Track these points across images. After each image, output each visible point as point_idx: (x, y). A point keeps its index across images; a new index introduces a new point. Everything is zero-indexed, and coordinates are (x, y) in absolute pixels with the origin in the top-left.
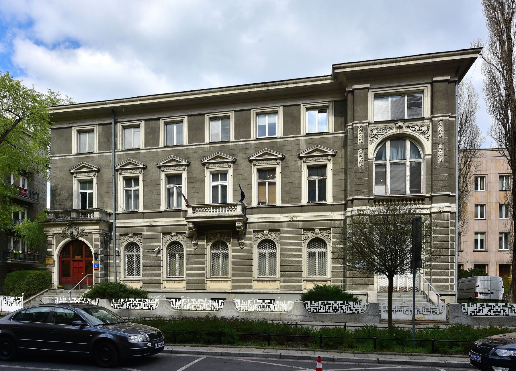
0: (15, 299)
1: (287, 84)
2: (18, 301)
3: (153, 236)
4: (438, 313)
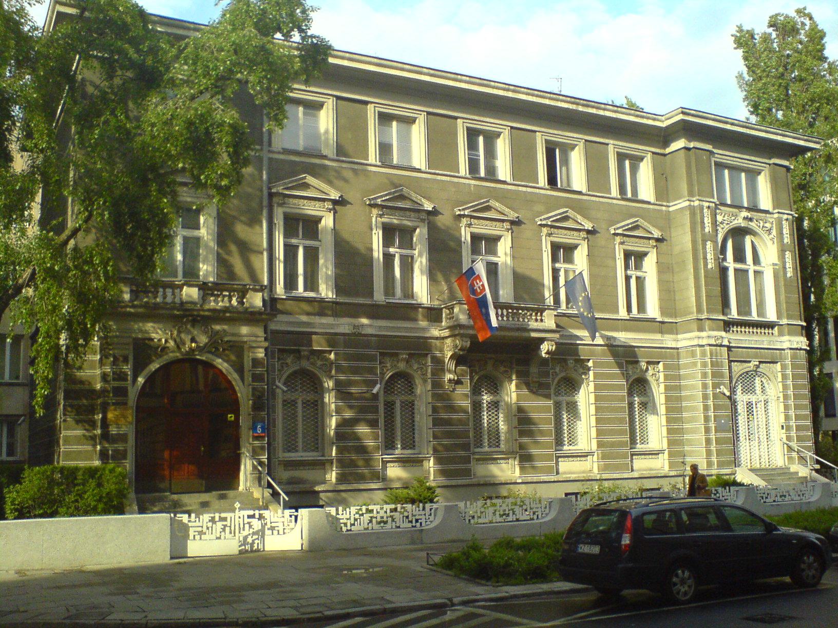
0: (212, 520)
2: (219, 525)
4: (281, 532)
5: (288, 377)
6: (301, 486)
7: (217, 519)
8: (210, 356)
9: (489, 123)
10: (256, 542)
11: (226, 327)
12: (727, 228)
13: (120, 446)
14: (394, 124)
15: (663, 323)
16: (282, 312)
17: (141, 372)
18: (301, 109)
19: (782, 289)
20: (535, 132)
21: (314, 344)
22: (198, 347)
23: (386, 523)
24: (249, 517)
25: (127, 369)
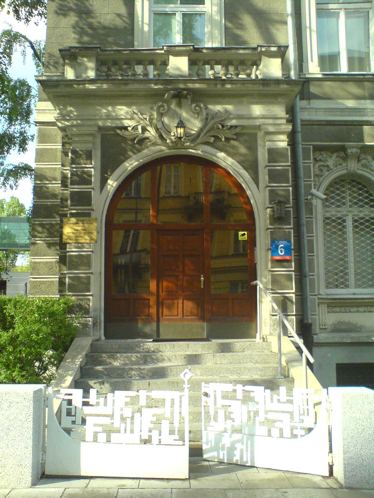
5: (330, 185)
6: (353, 335)
8: (208, 149)
10: (238, 446)
11: (230, 107)
13: (81, 273)
16: (317, 97)
17: (112, 172)
21: (366, 138)
22: (186, 134)
24: (225, 397)
25: (92, 168)
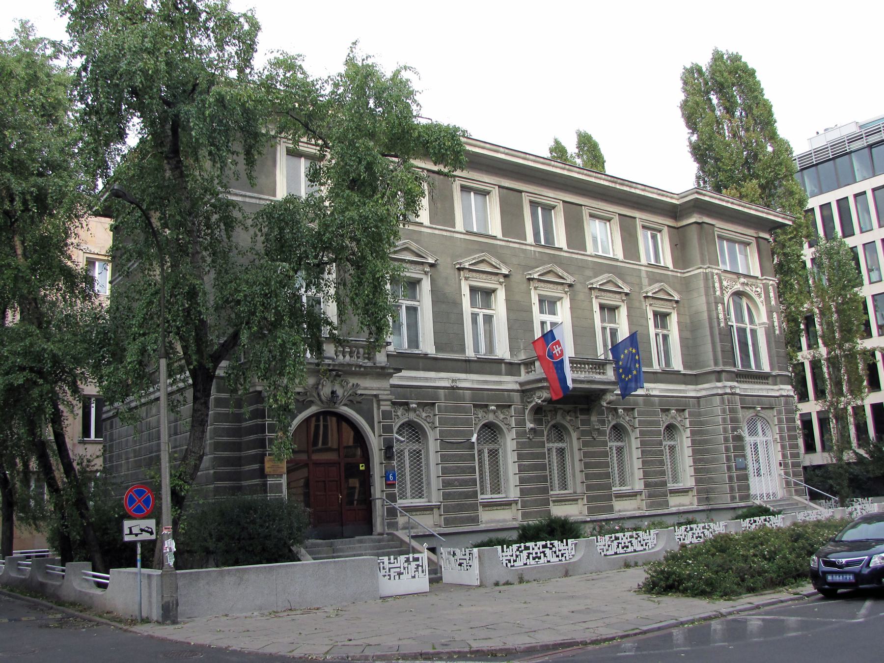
0: (407, 560)
1: (631, 187)
3: (457, 409)
7: (411, 559)
9: (549, 195)
12: (730, 292)
14: (303, 159)
15: (684, 375)
18: (472, 194)
19: (773, 345)
20: (521, 192)
23: (540, 558)
